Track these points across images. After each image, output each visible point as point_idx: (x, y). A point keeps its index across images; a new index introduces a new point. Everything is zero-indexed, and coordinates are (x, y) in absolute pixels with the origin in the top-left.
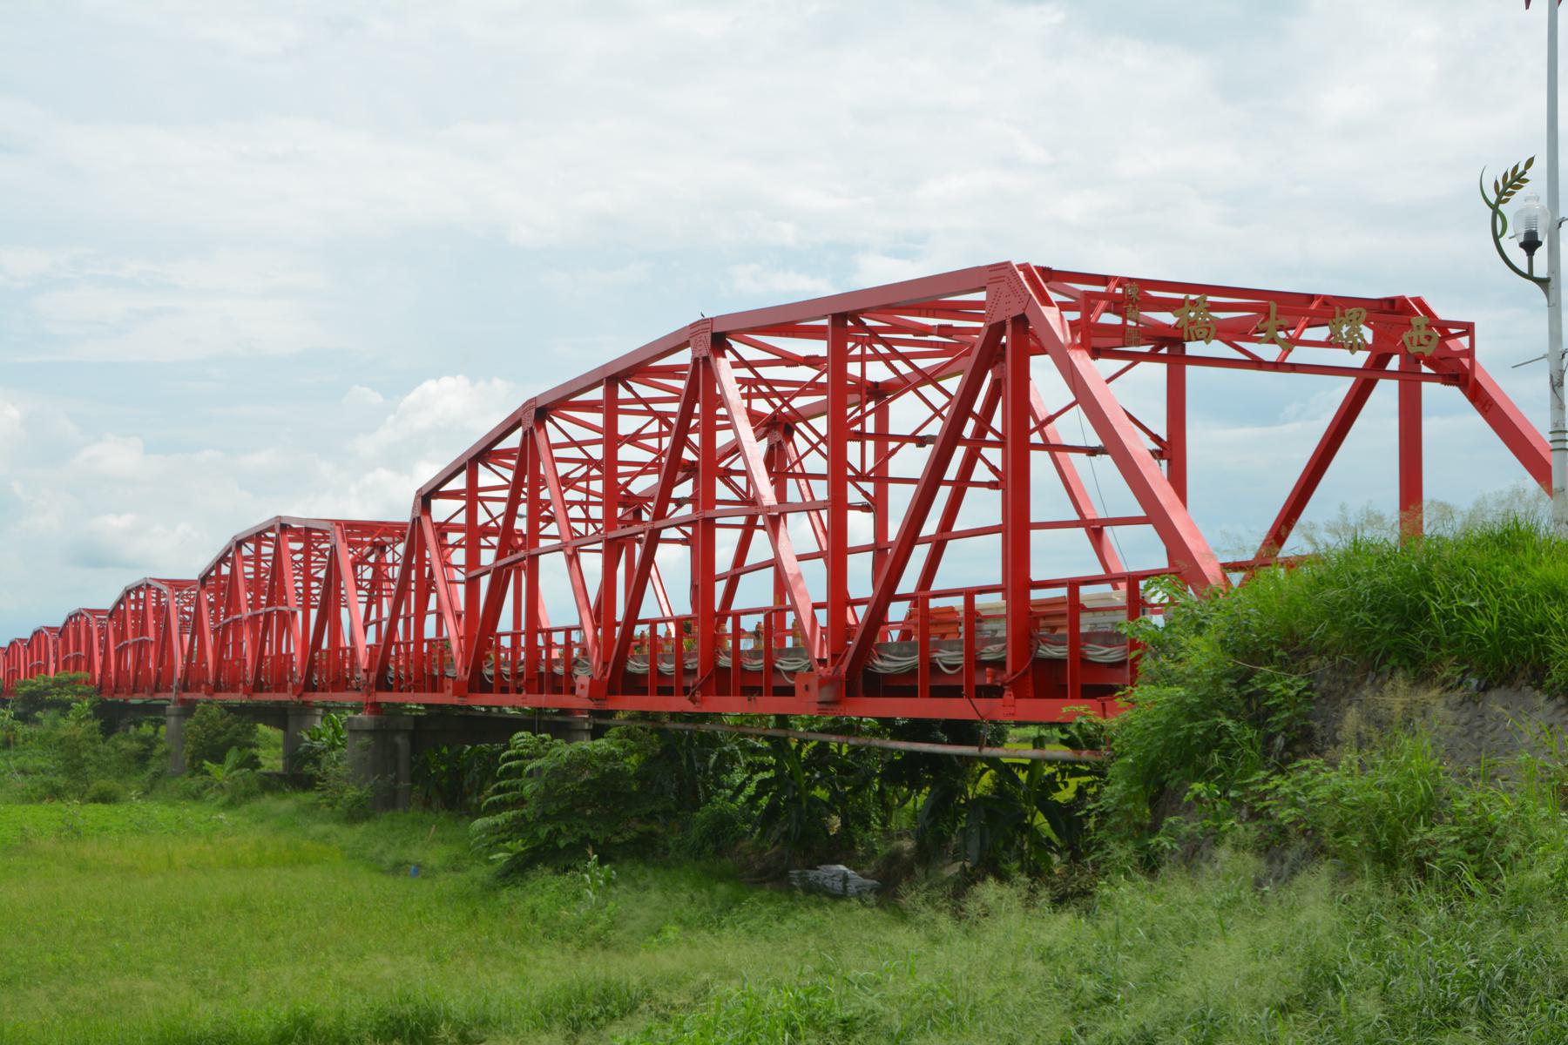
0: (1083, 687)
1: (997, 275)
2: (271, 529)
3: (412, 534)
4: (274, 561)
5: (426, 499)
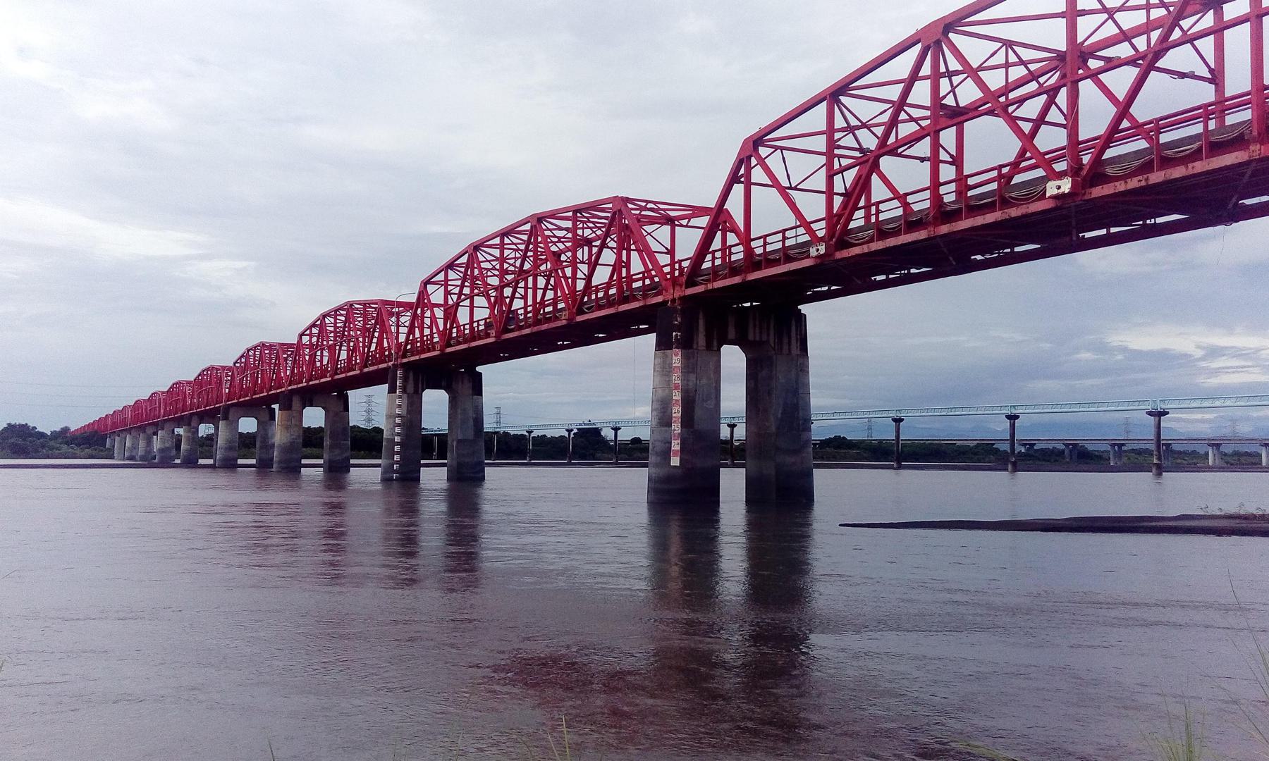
1: (614, 199)
2: (259, 346)
3: (299, 345)
5: (235, 364)
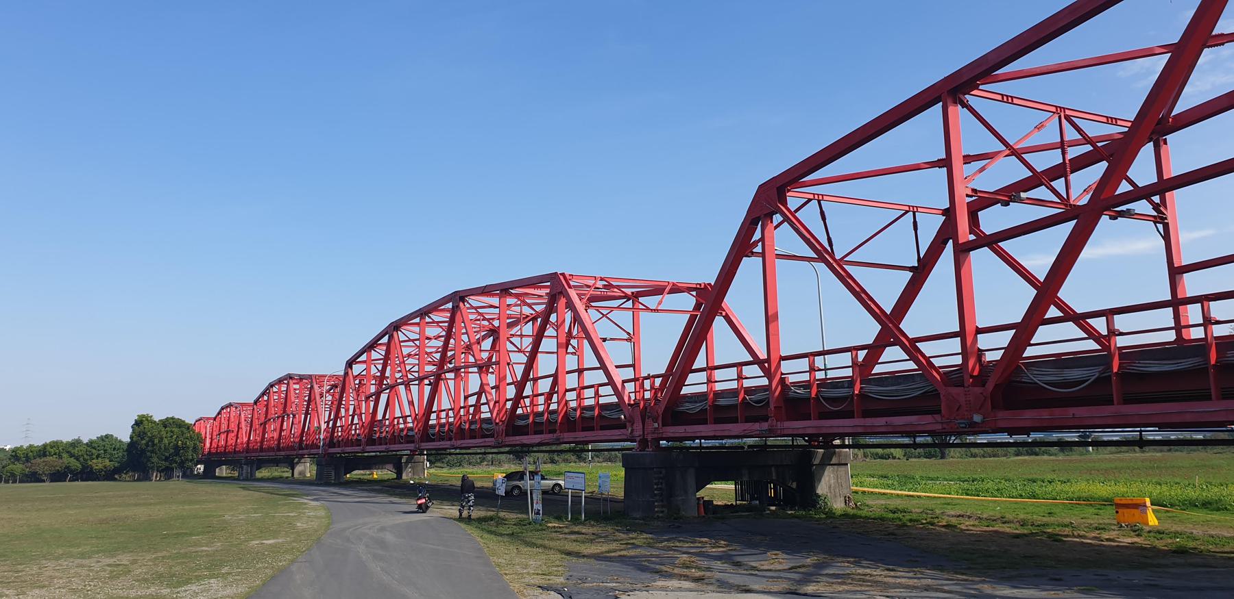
0: (601, 426)
4: (287, 393)
5: (350, 364)
